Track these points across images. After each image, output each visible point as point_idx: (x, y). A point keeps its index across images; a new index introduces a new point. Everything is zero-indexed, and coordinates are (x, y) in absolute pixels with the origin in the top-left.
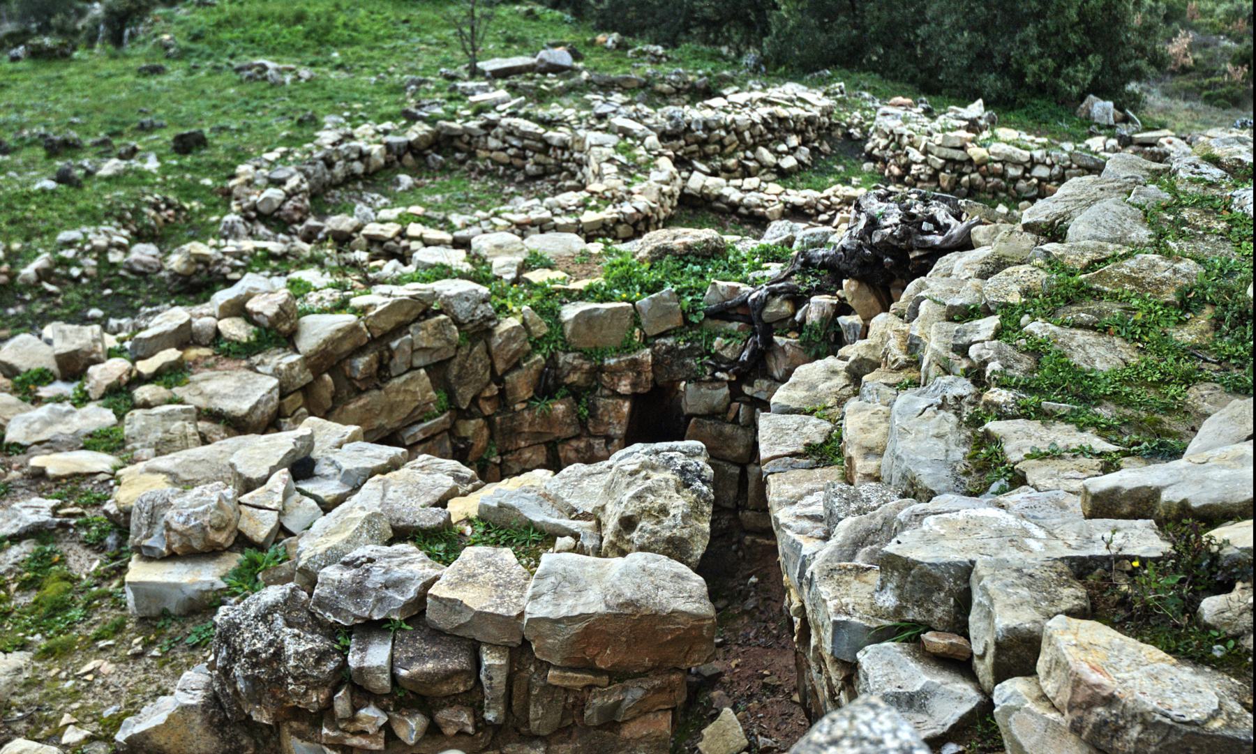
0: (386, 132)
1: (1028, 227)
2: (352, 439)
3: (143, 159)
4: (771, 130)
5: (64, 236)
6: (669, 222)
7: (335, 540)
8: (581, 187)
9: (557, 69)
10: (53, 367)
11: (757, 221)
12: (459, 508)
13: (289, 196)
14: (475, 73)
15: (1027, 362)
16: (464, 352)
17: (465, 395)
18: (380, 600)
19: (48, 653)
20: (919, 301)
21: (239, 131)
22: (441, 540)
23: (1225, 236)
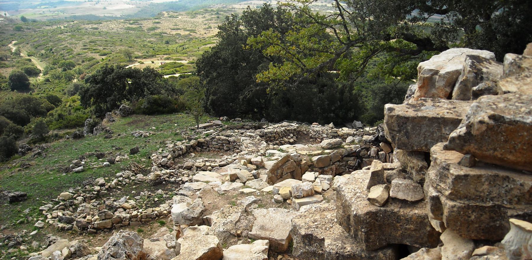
5: (118, 174)
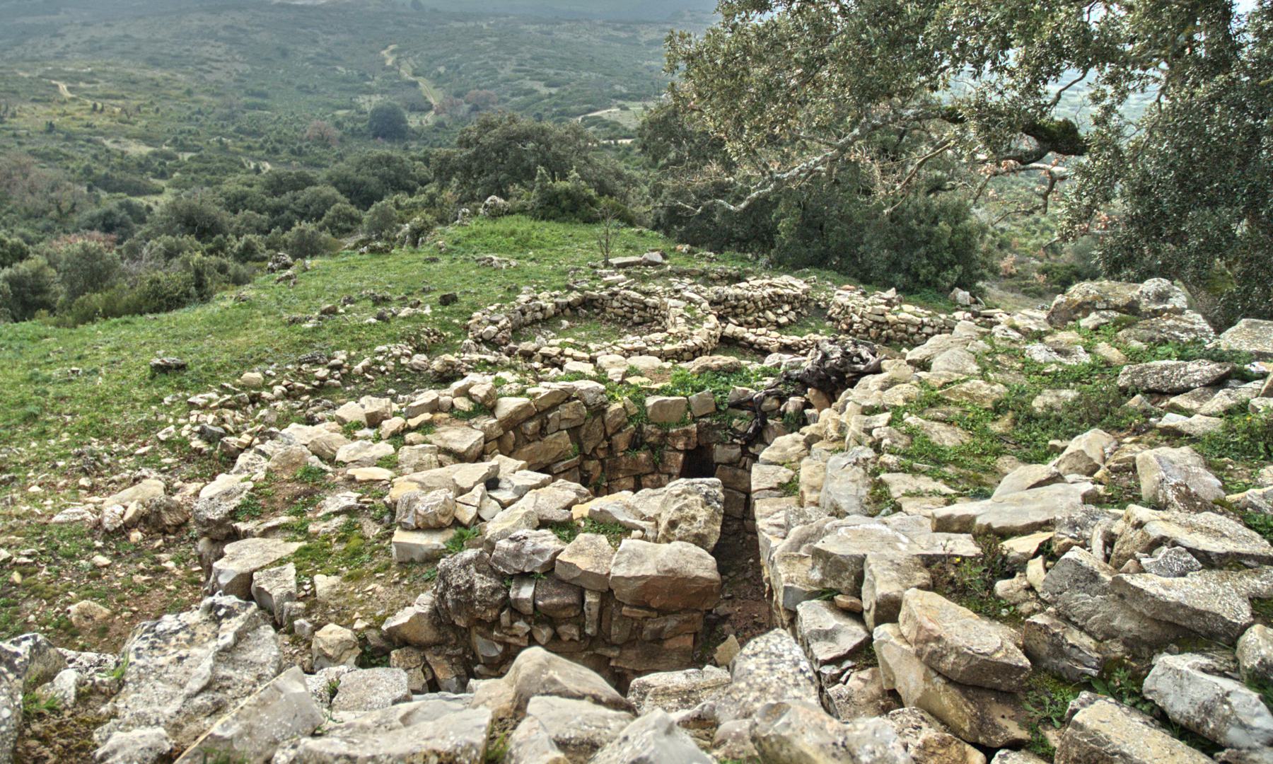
0: (556, 296)
1: (909, 362)
2: (521, 468)
3: (423, 308)
4: (774, 301)
5: (378, 348)
6: (713, 352)
7: (507, 525)
8: (664, 330)
9: (654, 264)
10: (364, 420)
11: (764, 352)
12: (579, 511)
13: (500, 330)
14: (607, 265)
15: (906, 440)
16: (589, 421)
17: (589, 446)
18: (529, 561)
19: (350, 578)
20: (846, 402)
21: (476, 294)
22: (565, 528)
23: (1021, 371)
